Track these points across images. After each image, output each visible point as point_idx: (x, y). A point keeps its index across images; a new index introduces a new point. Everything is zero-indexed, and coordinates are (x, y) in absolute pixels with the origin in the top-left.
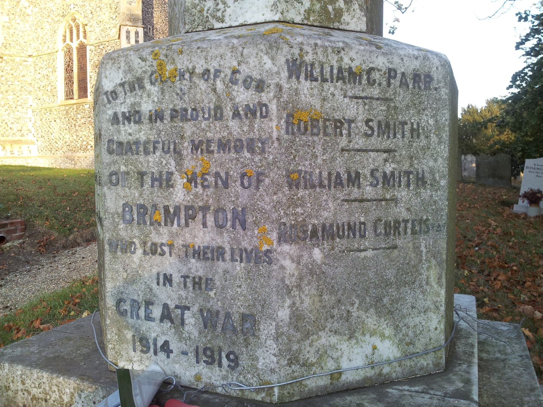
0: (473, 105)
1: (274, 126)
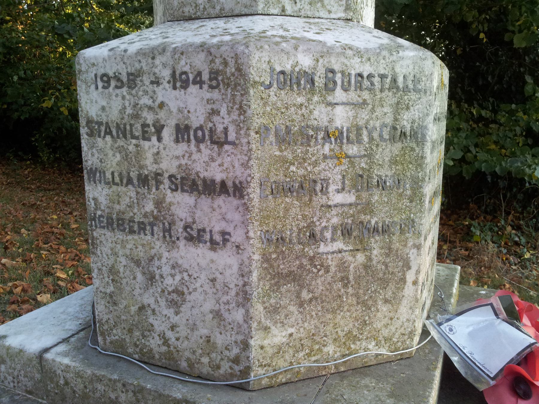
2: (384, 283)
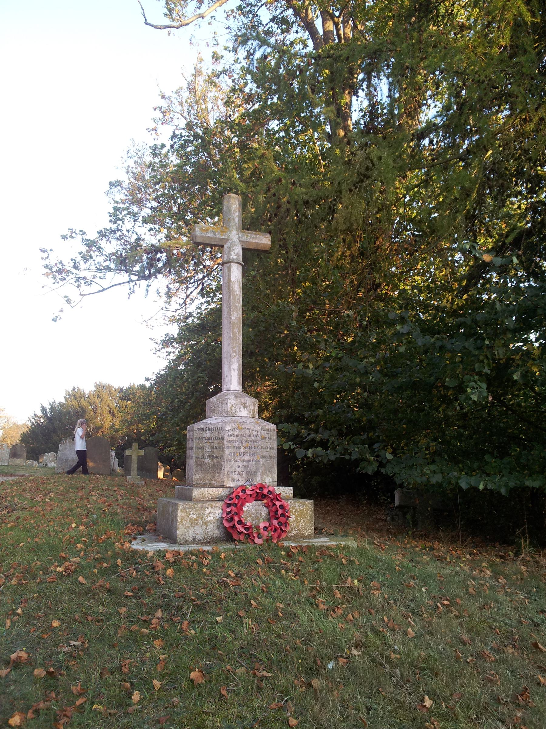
0: (81, 388)
1: (260, 438)
2: (217, 469)
